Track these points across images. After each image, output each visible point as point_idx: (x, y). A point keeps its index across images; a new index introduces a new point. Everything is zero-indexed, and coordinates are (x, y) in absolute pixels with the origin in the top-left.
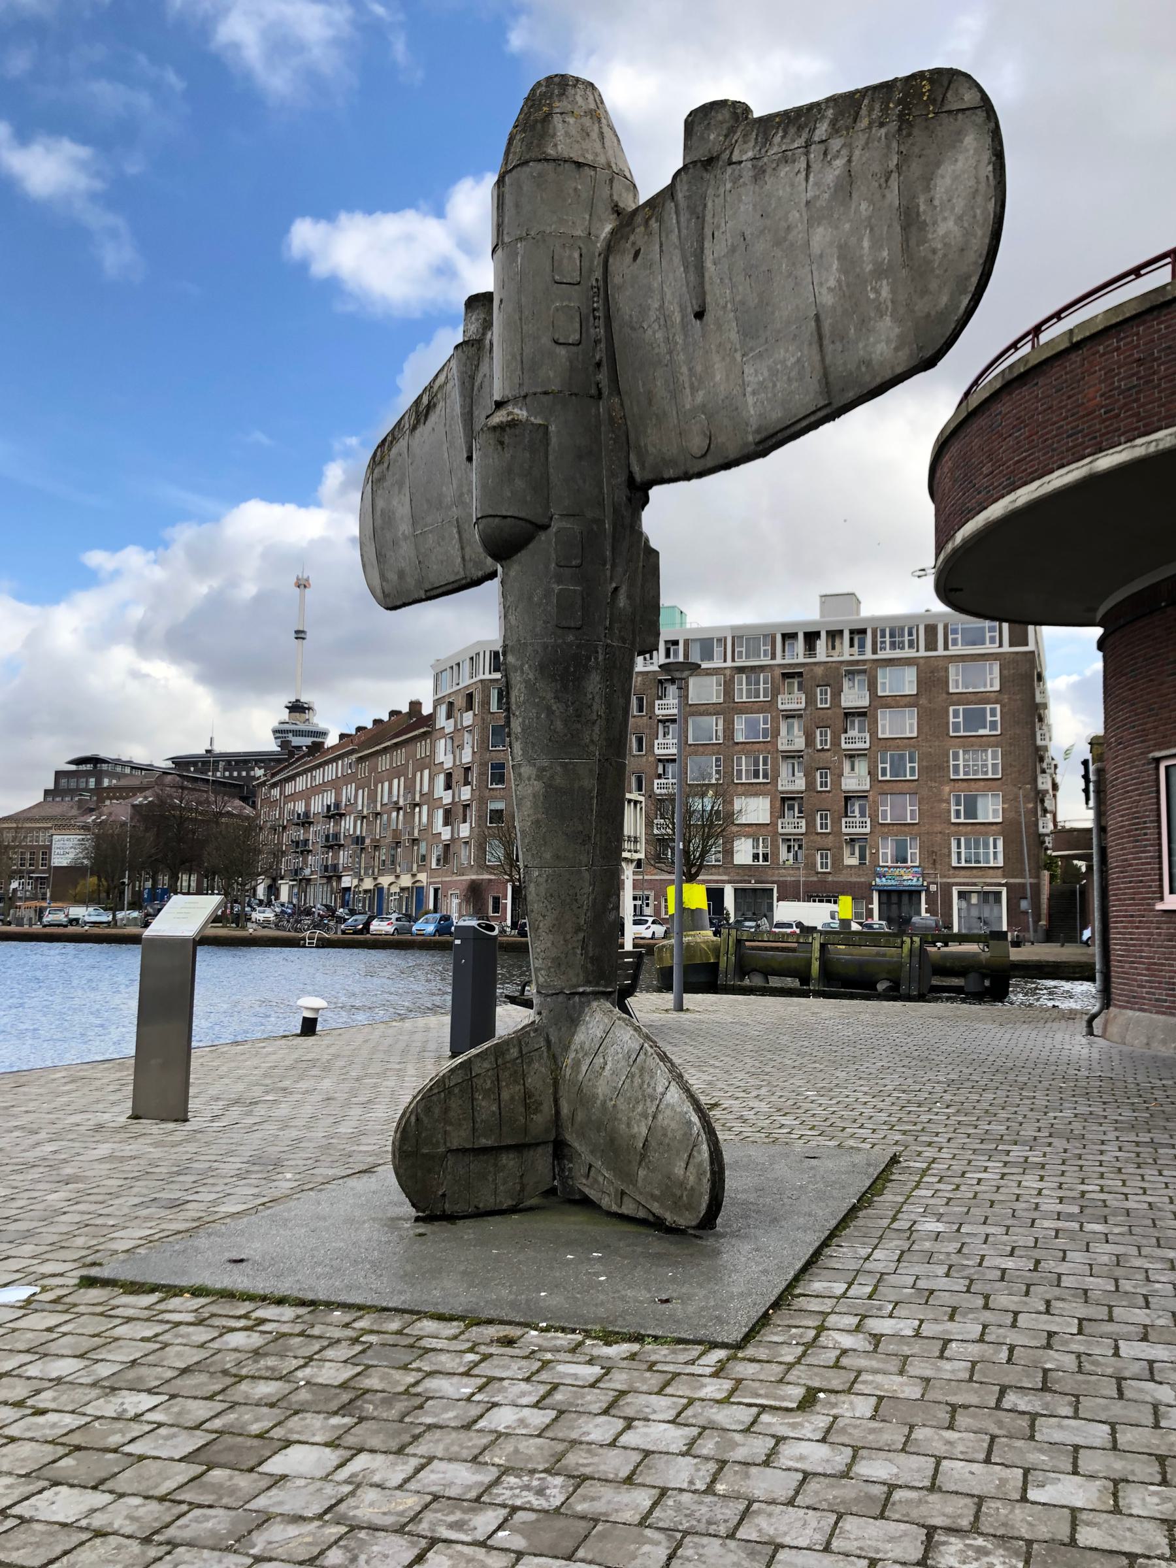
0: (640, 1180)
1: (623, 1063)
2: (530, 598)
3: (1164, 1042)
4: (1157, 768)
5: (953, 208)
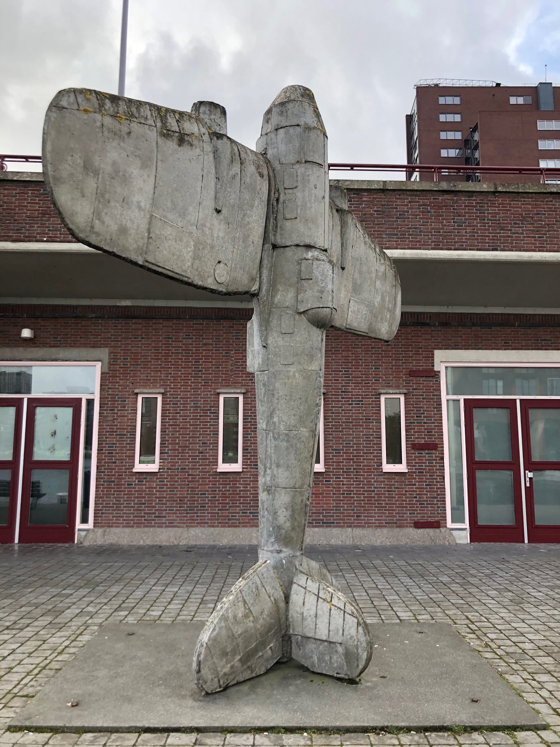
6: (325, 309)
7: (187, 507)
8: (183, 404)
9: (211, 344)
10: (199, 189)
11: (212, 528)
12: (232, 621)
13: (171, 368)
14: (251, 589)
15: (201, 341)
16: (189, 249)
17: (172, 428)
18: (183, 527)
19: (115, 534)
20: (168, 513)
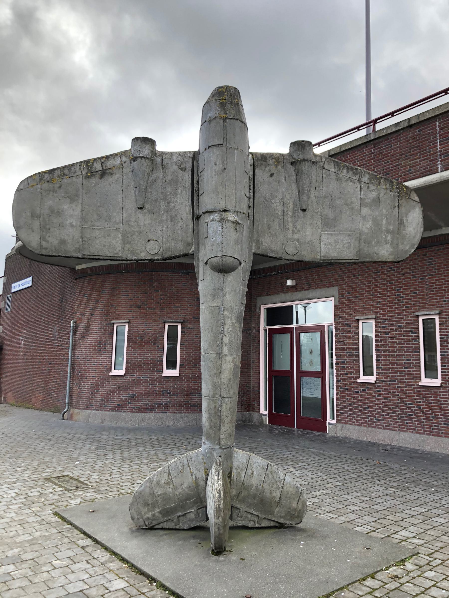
0: (276, 512)
1: (261, 471)
2: (235, 291)
3: (110, 421)
4: (113, 326)
5: (412, 225)
6: (216, 258)
7: (398, 414)
8: (391, 326)
9: (408, 273)
10: (120, 200)
11: (418, 435)
12: (156, 484)
13: (380, 297)
14: (177, 466)
15: (401, 272)
16: (117, 239)
17: (383, 347)
18: (397, 431)
19: (349, 429)
20: (385, 418)
